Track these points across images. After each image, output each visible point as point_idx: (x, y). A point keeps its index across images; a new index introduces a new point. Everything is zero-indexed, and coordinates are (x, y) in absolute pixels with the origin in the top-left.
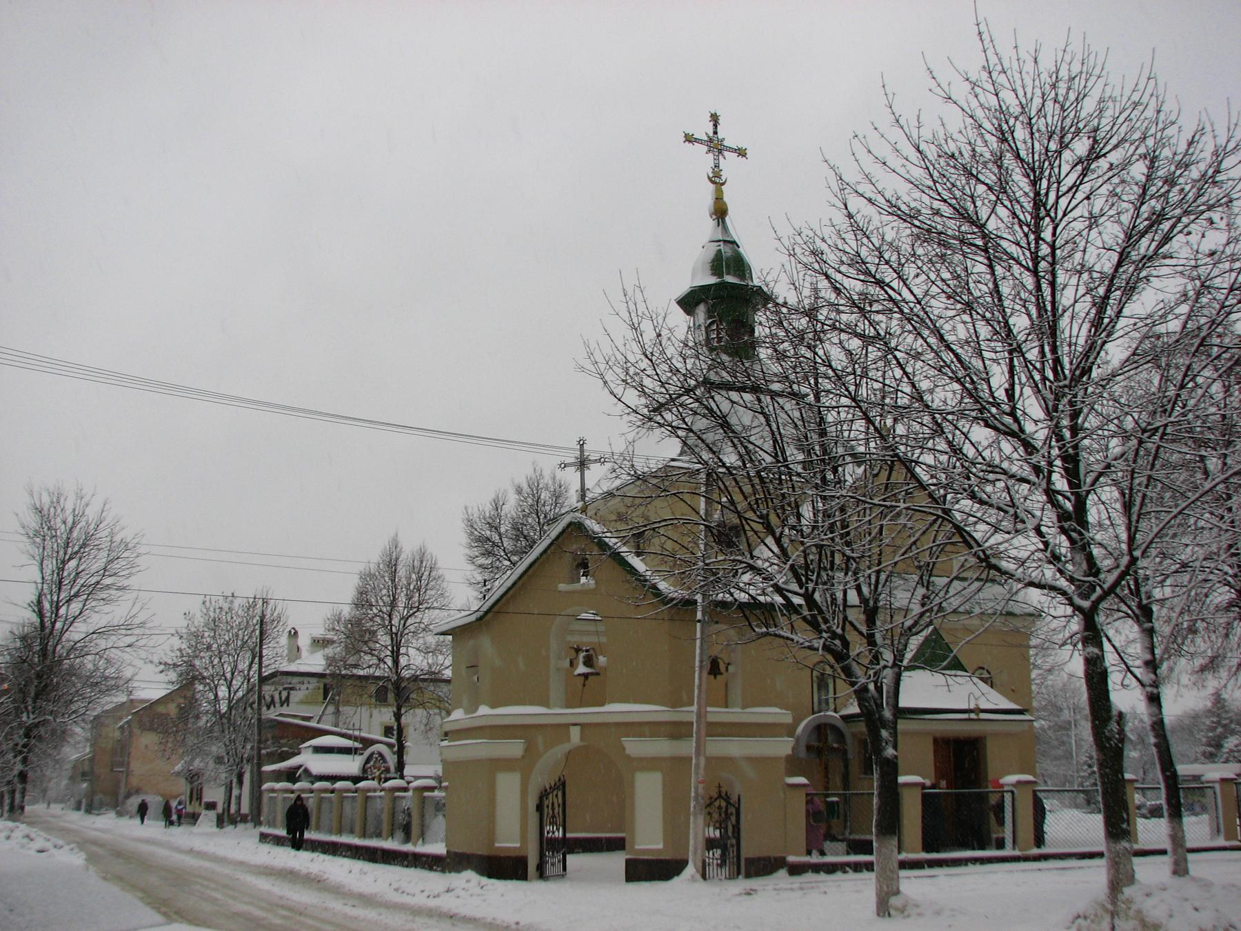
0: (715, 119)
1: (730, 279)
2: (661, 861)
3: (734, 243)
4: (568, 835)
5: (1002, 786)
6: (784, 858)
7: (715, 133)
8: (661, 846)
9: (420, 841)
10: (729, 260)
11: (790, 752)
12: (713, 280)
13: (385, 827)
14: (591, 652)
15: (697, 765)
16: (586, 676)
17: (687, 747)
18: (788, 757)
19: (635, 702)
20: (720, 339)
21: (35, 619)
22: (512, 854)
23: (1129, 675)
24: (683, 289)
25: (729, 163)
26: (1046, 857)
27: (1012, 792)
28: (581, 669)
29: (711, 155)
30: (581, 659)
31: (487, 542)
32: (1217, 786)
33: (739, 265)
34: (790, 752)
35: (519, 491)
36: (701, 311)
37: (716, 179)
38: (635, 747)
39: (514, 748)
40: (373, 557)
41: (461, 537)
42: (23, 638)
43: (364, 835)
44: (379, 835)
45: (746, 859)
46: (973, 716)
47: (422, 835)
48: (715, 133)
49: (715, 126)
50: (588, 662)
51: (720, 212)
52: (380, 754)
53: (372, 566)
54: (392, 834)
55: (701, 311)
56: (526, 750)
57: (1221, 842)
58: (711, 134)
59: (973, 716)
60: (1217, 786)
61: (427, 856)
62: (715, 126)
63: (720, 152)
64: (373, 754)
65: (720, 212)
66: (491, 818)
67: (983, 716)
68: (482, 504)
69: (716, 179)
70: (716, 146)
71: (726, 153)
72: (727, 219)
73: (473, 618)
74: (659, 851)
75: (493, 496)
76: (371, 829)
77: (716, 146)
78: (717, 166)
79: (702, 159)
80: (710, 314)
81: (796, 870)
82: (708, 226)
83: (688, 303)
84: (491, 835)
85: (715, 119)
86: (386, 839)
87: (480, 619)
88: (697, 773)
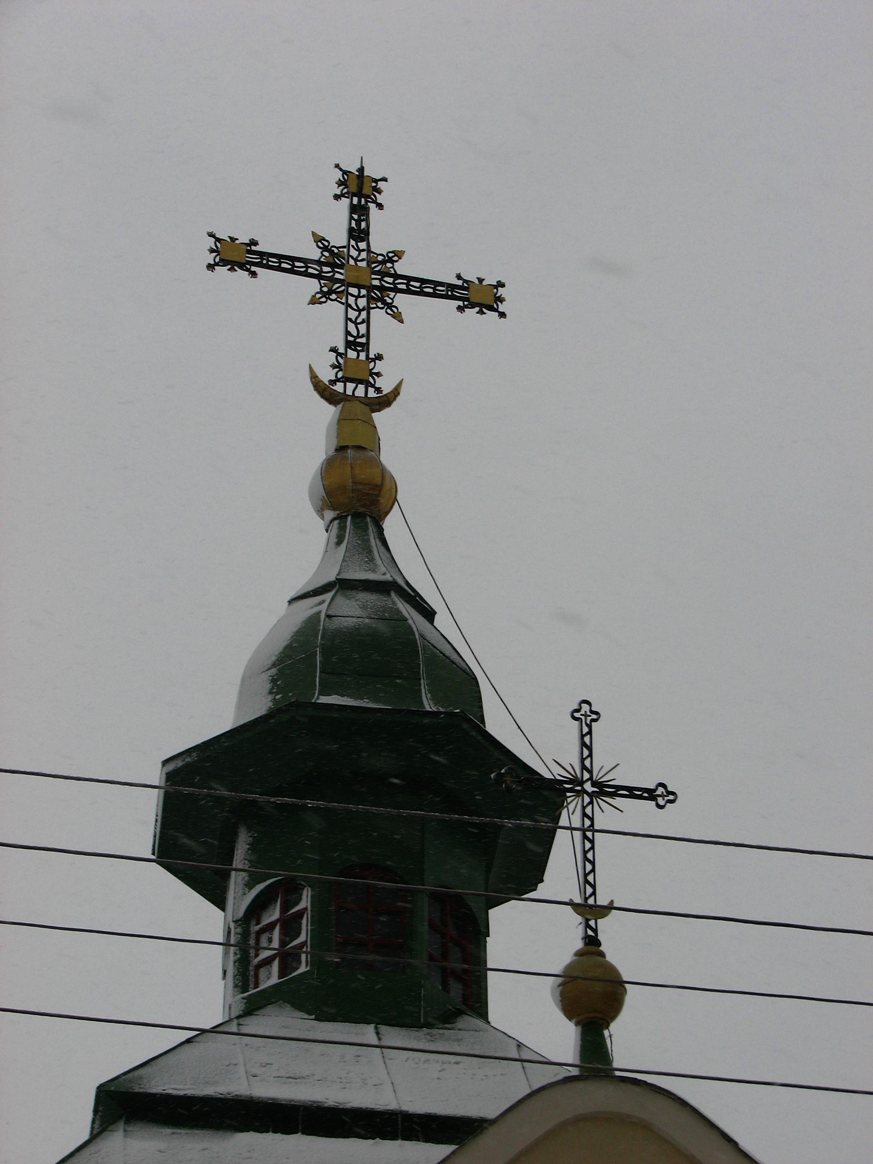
4: (233, 873)
7: (358, 234)
20: (287, 959)
23: (525, 1064)
25: (411, 341)
29: (334, 310)
37: (355, 392)
42: (270, 693)
48: (358, 234)
49: (359, 212)
51: (357, 497)
58: (338, 237)
62: (359, 212)
65: (357, 497)
69: (355, 392)
70: (358, 275)
71: (401, 301)
72: (392, 525)
77: (358, 275)
79: (306, 327)
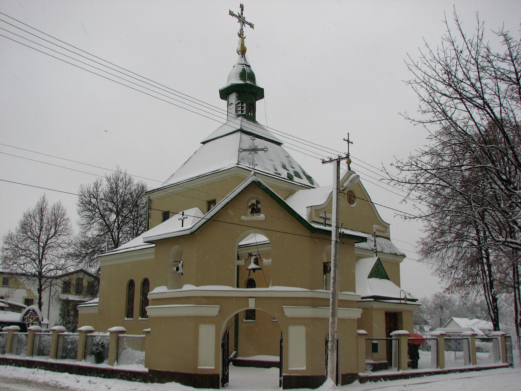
0: (242, 7)
1: (248, 82)
2: (304, 377)
3: (249, 66)
5: (391, 336)
6: (357, 374)
7: (242, 14)
8: (304, 368)
9: (116, 363)
10: (247, 74)
11: (360, 316)
12: (241, 82)
13: (80, 350)
14: (258, 256)
15: (333, 322)
16: (254, 270)
17: (325, 312)
18: (358, 319)
19: (285, 285)
21: (481, 81)
22: (210, 373)
24: (224, 84)
26: (445, 373)
27: (437, 339)
28: (253, 266)
29: (239, 24)
30: (252, 260)
31: (90, 204)
32: (469, 338)
33: (252, 77)
34: (360, 316)
35: (109, 180)
36: (233, 98)
37: (241, 35)
38: (290, 311)
39: (213, 310)
40: (32, 206)
41: (76, 200)
43: (56, 357)
44: (75, 357)
45: (342, 375)
46: (403, 302)
47: (117, 359)
49: (242, 10)
50: (256, 262)
52: (34, 311)
53: (30, 210)
54: (85, 357)
55: (233, 98)
56: (219, 312)
57: (501, 363)
59: (403, 302)
60: (499, 338)
61: (10, 359)
62: (242, 10)
63: (243, 23)
64: (29, 310)
65: (243, 51)
66: (196, 353)
67: (408, 302)
68: (89, 183)
69: (241, 35)
73: (188, 232)
74: (303, 371)
75: (95, 181)
76: (60, 353)
78: (242, 29)
80: (238, 98)
81: (363, 380)
82: (237, 58)
83: (225, 94)
84: (196, 362)
85: (242, 7)
86: (81, 361)
87: (191, 234)
88: (333, 328)
